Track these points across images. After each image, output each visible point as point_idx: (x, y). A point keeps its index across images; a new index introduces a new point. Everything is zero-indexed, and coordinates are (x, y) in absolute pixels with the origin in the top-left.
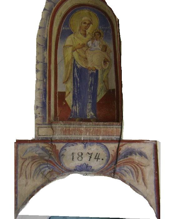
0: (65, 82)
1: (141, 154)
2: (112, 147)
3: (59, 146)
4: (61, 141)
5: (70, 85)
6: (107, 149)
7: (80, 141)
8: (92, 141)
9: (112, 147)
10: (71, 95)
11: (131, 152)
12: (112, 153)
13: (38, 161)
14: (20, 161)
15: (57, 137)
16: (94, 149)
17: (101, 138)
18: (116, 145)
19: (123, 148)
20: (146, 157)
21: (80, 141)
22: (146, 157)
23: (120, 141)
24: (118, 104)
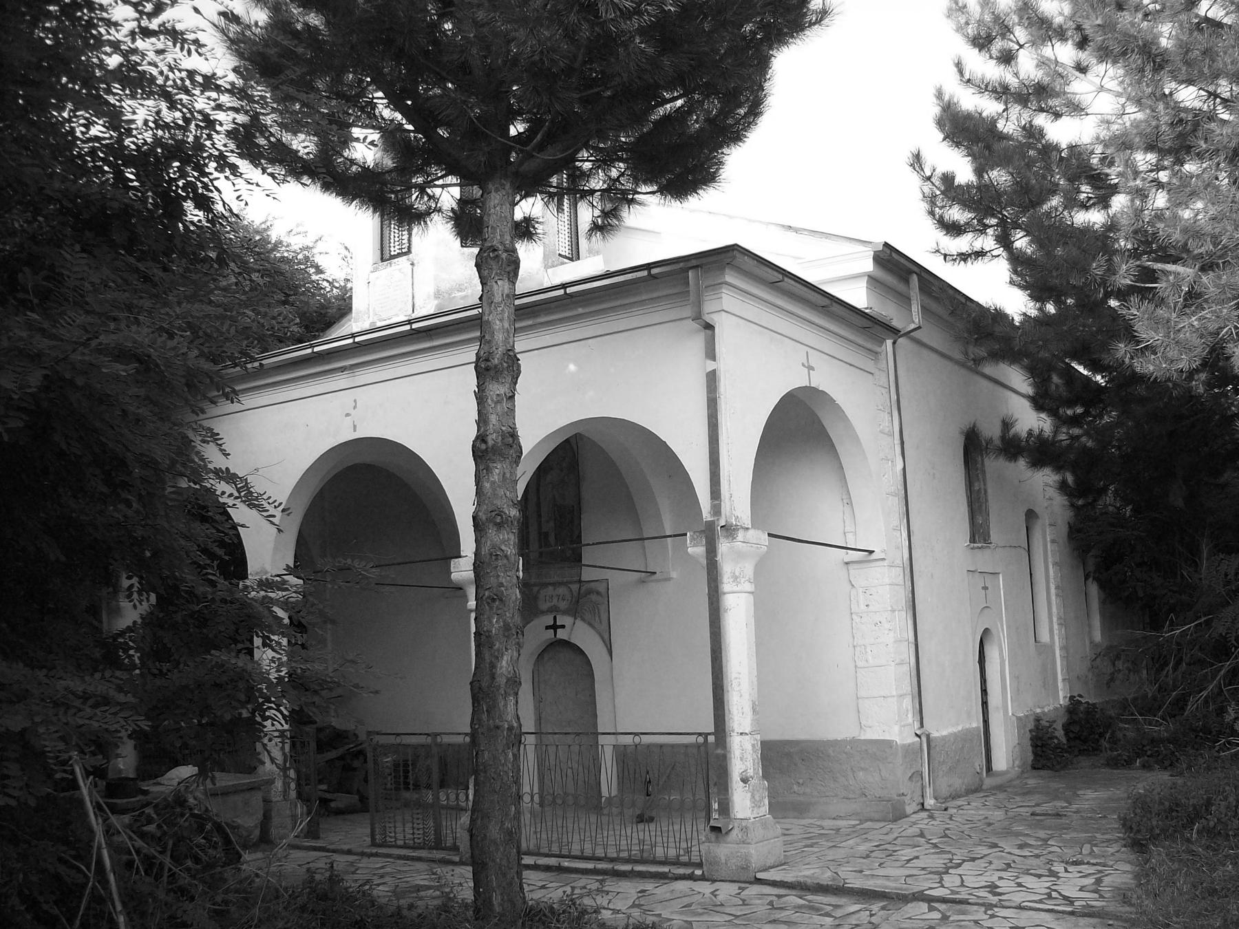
0: (548, 522)
1: (598, 593)
2: (575, 587)
3: (536, 589)
4: (535, 585)
5: (552, 524)
6: (571, 590)
7: (550, 584)
8: (561, 584)
9: (575, 587)
10: (553, 534)
11: (590, 592)
12: (575, 594)
13: (263, 91)
14: (951, 292)
15: (533, 581)
16: (562, 590)
17: (565, 580)
18: (578, 586)
19: (583, 589)
20: (602, 596)
21: (550, 584)
22: (602, 596)
23: (580, 581)
24: (936, 283)
